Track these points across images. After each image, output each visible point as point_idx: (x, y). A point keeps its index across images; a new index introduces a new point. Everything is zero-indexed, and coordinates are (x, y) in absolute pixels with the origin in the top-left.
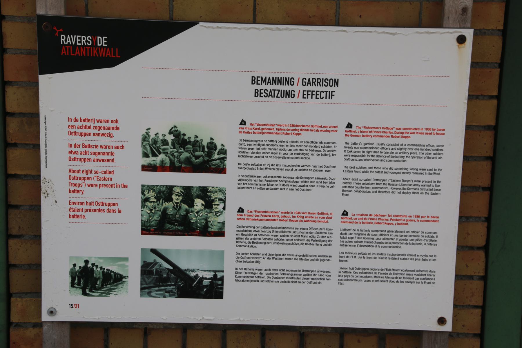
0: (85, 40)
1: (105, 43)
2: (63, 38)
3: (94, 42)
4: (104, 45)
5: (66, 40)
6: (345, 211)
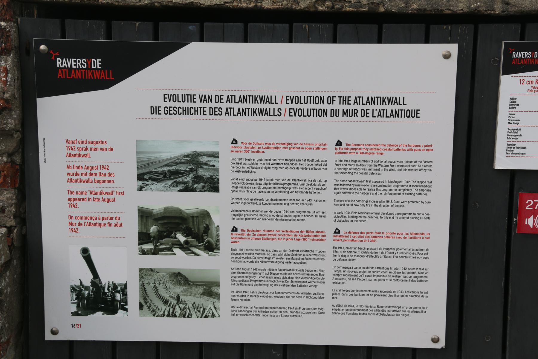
0: (80, 63)
1: (100, 66)
2: (59, 61)
3: (89, 64)
4: (98, 67)
5: (62, 64)
6: (337, 229)
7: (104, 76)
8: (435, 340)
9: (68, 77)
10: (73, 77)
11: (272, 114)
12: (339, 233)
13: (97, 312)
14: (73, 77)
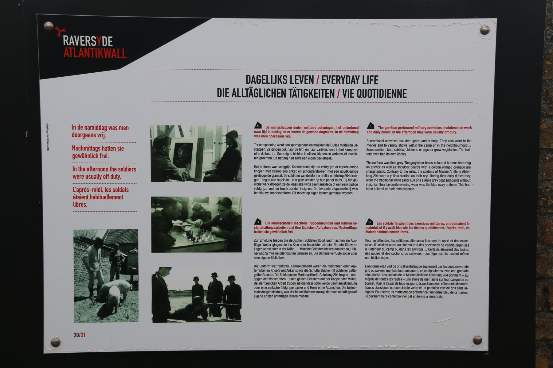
0: (89, 40)
1: (111, 43)
2: (66, 38)
3: (99, 42)
4: (109, 45)
6: (369, 220)
7: (115, 55)
8: (477, 342)
9: (75, 56)
10: (81, 56)
11: (240, 94)
12: (372, 224)
13: (152, 315)
14: (81, 56)
